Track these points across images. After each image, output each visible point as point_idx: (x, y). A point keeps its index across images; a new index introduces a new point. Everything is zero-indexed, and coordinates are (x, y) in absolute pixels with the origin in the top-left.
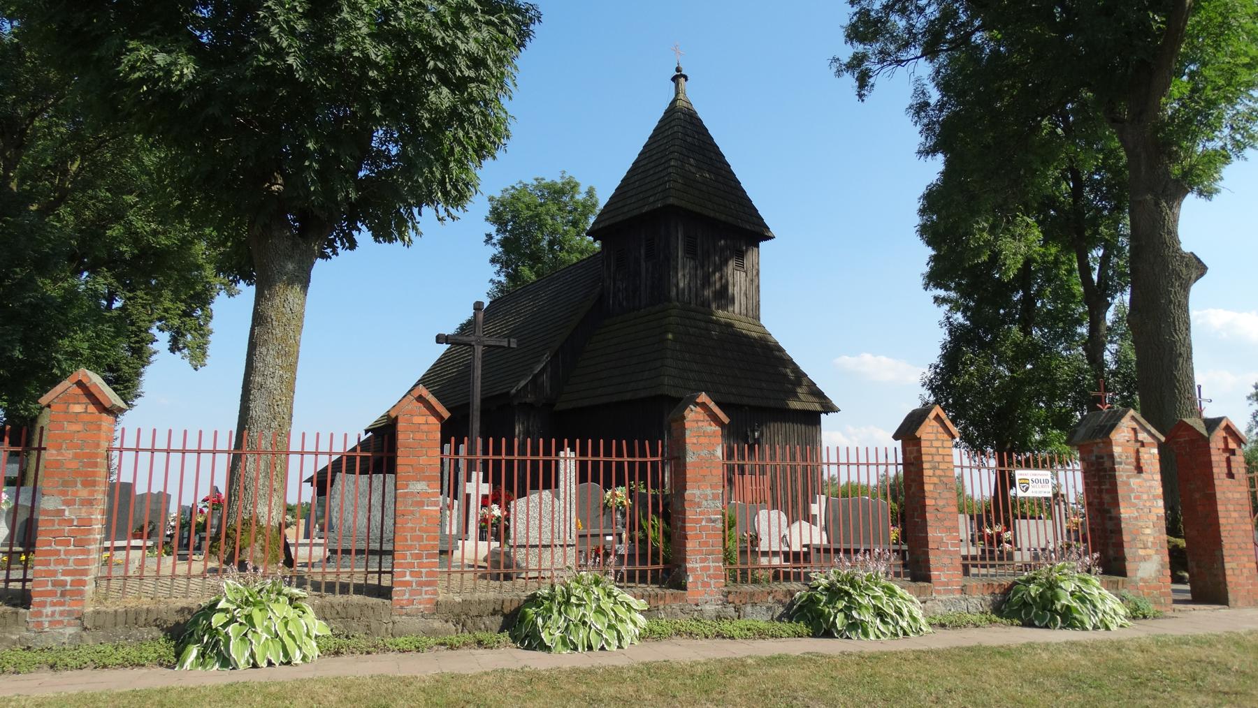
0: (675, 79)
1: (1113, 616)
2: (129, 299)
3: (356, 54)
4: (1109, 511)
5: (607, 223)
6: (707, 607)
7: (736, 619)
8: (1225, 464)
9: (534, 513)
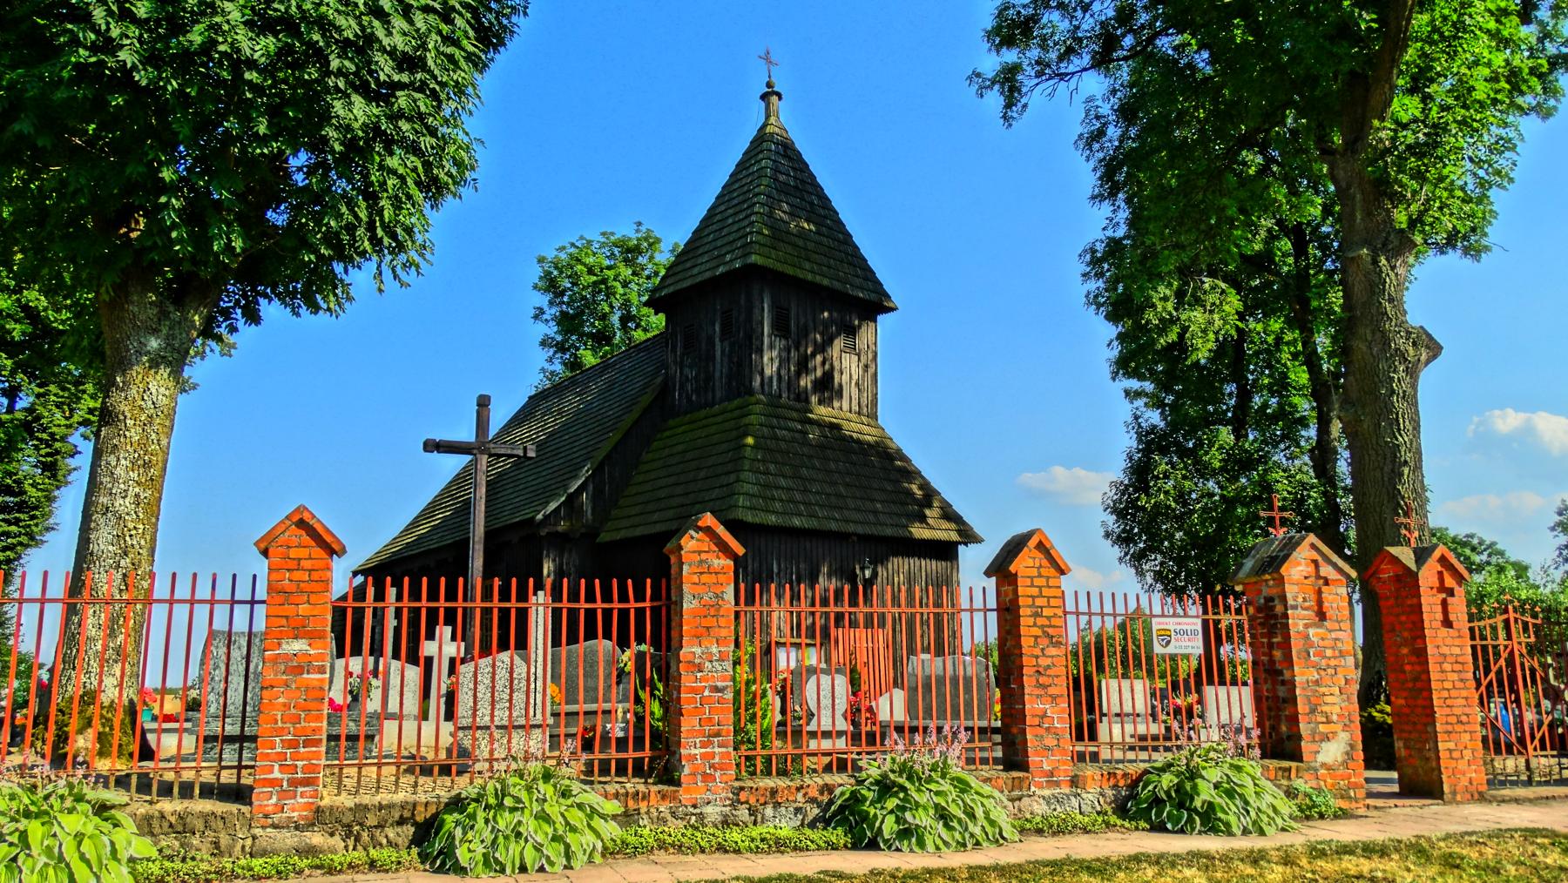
0: (764, 97)
1: (1272, 815)
2: (38, 396)
3: (222, 48)
4: (1281, 673)
5: (671, 289)
6: (708, 810)
7: (751, 826)
8: (1439, 608)
9: (485, 680)
